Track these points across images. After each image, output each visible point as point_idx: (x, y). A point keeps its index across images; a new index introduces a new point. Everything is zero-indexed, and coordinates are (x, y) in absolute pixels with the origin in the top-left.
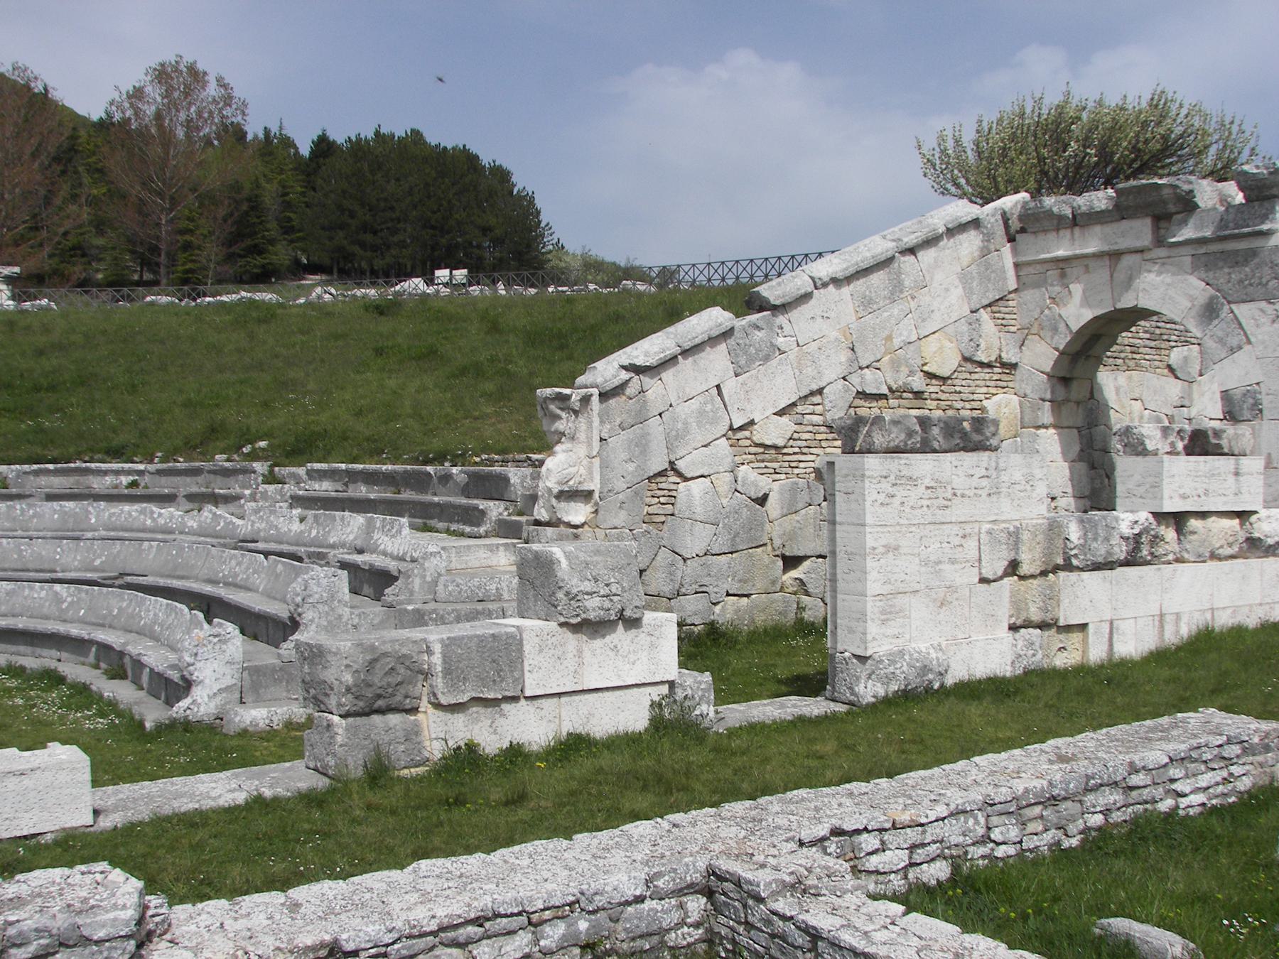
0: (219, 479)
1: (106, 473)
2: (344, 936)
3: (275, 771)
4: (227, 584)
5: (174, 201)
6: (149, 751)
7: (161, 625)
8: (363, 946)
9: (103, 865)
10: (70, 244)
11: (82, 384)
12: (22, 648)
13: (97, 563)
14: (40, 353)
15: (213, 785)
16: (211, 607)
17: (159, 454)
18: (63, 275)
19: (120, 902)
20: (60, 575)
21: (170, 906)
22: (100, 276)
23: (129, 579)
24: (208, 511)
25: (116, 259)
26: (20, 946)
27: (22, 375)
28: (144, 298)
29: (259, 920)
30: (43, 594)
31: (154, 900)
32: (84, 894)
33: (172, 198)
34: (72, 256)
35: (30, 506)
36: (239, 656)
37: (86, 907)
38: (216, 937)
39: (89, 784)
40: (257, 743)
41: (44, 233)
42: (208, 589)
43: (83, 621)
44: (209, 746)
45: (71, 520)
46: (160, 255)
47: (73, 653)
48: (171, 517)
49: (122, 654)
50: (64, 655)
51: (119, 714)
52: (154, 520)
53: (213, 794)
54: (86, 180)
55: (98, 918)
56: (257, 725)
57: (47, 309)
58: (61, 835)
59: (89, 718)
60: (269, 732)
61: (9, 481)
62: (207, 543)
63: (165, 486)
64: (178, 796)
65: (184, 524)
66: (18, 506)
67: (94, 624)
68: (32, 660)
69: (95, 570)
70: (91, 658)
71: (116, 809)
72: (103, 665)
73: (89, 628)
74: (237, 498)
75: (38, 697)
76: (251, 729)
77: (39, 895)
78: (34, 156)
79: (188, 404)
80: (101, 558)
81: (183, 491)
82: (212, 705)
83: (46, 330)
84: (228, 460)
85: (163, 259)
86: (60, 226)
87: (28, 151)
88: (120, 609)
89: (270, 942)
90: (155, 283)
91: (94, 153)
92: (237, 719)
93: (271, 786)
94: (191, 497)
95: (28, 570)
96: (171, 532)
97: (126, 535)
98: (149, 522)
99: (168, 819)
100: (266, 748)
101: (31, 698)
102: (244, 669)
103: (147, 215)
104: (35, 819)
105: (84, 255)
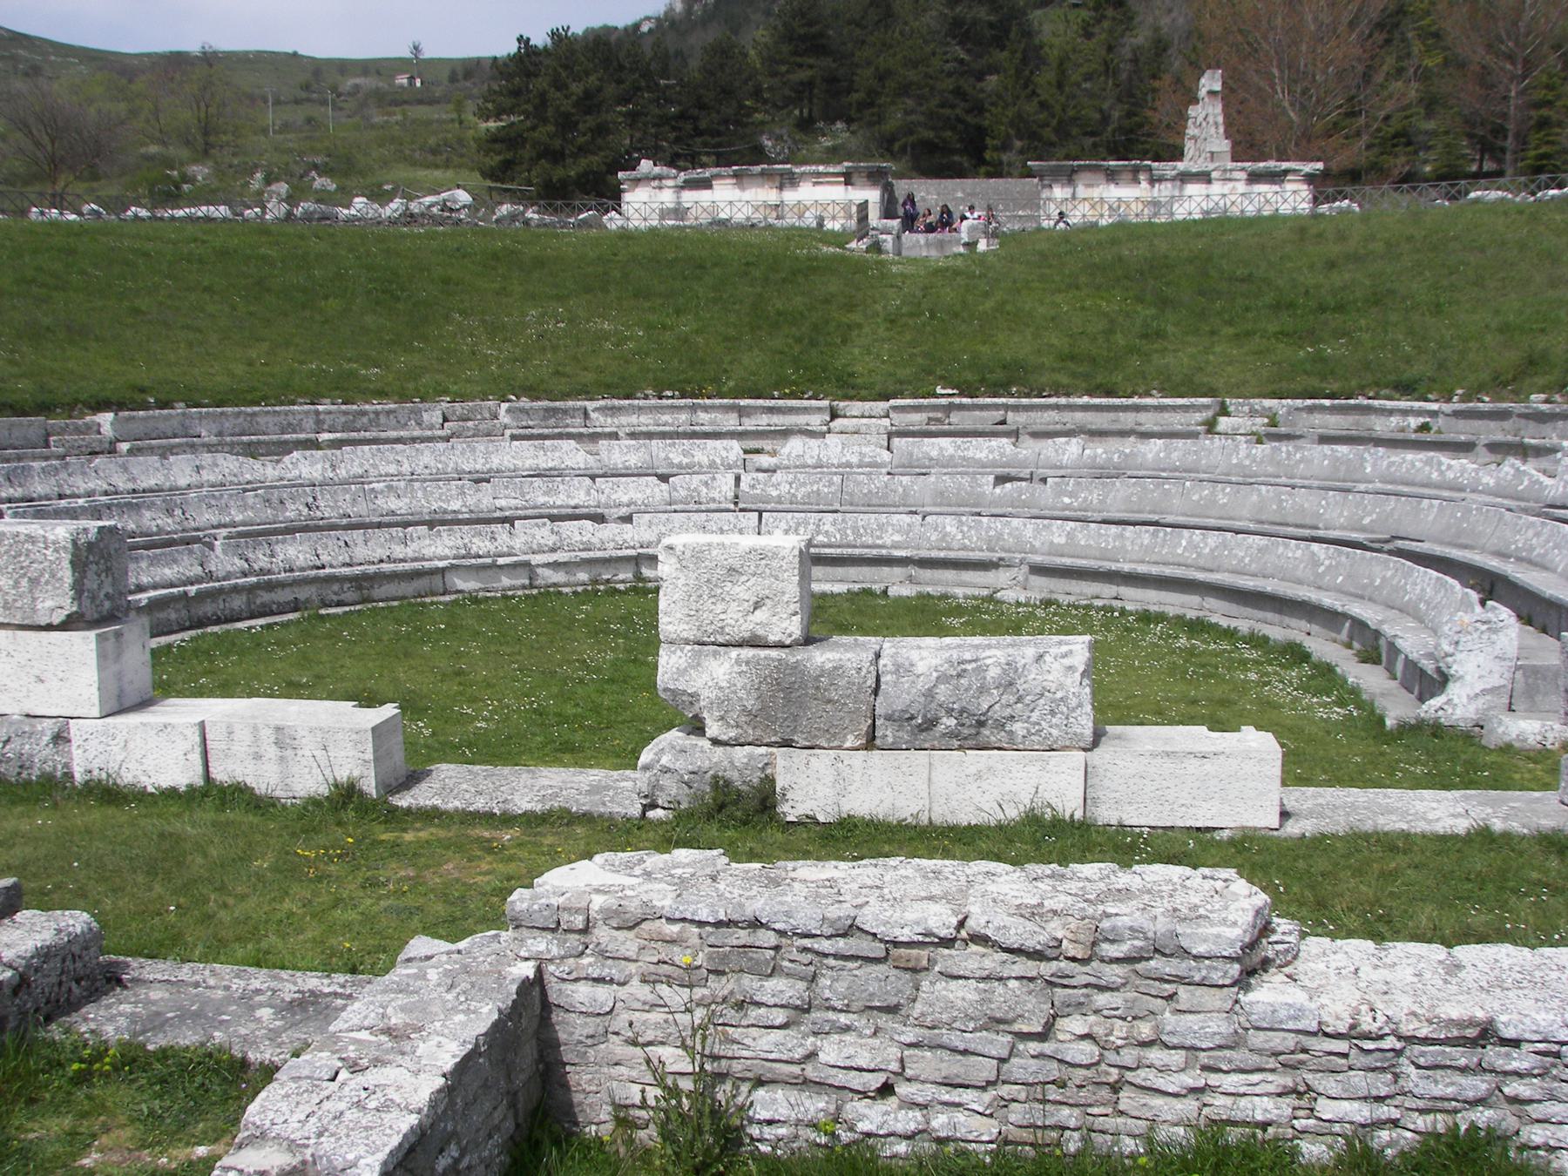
0: (1532, 424)
1: (1391, 412)
2: (1503, 1018)
3: (1516, 799)
4: (1519, 559)
5: (1528, 65)
6: (1382, 754)
7: (1428, 603)
8: (1527, 1036)
9: (1230, 873)
10: (1391, 130)
11: (1376, 303)
12: (1270, 616)
13: (1366, 521)
14: (1331, 265)
15: (1434, 805)
16: (1491, 586)
17: (1460, 391)
18: (1381, 170)
19: (1231, 918)
20: (1321, 533)
21: (1303, 935)
22: (1428, 169)
23: (1399, 543)
24: (1511, 465)
25: (1448, 145)
26: (1113, 942)
27: (1307, 292)
28: (1467, 193)
29: (1405, 974)
30: (1299, 553)
31: (1283, 925)
32: (1196, 900)
33: (1526, 61)
34: (1394, 146)
35: (1297, 449)
36: (1512, 651)
37: (1193, 915)
38: (1343, 983)
39: (1278, 781)
40: (1521, 763)
41: (1362, 120)
42: (1493, 564)
43: (1340, 590)
44: (1456, 756)
45: (1343, 468)
46: (1506, 137)
47: (1324, 626)
48: (1463, 470)
49: (1377, 634)
50: (1315, 628)
51: (1360, 705)
52: (1442, 473)
53: (1431, 816)
54: (1417, 47)
55: (1200, 930)
56: (1525, 740)
57: (1348, 211)
58: (1239, 834)
59: (1325, 705)
60: (1539, 752)
61: (1278, 418)
62: (1502, 506)
63: (1461, 431)
64: (1388, 811)
65: (1478, 481)
66: (1285, 447)
67: (1352, 595)
68: (1278, 630)
69: (1363, 529)
70: (1344, 635)
71: (1310, 814)
72: (1356, 645)
73: (1345, 599)
74: (1553, 450)
75: (1276, 673)
76: (1517, 745)
77: (1149, 892)
78: (1352, 25)
79: (1504, 329)
80: (1370, 515)
81: (1484, 439)
82: (1472, 708)
83: (1342, 237)
84: (1547, 401)
85: (1510, 143)
86: (1380, 108)
87: (1346, 18)
88: (1384, 579)
89: (1406, 1003)
90: (1500, 174)
91: (1428, 13)
92: (1500, 730)
93: (1505, 819)
94: (1493, 447)
95: (1287, 525)
96: (1461, 489)
97: (1406, 489)
98: (1435, 475)
99: (1366, 836)
100: (1530, 771)
101: (1267, 674)
102: (1518, 668)
103: (1493, 86)
104: (1214, 810)
105: (1409, 144)
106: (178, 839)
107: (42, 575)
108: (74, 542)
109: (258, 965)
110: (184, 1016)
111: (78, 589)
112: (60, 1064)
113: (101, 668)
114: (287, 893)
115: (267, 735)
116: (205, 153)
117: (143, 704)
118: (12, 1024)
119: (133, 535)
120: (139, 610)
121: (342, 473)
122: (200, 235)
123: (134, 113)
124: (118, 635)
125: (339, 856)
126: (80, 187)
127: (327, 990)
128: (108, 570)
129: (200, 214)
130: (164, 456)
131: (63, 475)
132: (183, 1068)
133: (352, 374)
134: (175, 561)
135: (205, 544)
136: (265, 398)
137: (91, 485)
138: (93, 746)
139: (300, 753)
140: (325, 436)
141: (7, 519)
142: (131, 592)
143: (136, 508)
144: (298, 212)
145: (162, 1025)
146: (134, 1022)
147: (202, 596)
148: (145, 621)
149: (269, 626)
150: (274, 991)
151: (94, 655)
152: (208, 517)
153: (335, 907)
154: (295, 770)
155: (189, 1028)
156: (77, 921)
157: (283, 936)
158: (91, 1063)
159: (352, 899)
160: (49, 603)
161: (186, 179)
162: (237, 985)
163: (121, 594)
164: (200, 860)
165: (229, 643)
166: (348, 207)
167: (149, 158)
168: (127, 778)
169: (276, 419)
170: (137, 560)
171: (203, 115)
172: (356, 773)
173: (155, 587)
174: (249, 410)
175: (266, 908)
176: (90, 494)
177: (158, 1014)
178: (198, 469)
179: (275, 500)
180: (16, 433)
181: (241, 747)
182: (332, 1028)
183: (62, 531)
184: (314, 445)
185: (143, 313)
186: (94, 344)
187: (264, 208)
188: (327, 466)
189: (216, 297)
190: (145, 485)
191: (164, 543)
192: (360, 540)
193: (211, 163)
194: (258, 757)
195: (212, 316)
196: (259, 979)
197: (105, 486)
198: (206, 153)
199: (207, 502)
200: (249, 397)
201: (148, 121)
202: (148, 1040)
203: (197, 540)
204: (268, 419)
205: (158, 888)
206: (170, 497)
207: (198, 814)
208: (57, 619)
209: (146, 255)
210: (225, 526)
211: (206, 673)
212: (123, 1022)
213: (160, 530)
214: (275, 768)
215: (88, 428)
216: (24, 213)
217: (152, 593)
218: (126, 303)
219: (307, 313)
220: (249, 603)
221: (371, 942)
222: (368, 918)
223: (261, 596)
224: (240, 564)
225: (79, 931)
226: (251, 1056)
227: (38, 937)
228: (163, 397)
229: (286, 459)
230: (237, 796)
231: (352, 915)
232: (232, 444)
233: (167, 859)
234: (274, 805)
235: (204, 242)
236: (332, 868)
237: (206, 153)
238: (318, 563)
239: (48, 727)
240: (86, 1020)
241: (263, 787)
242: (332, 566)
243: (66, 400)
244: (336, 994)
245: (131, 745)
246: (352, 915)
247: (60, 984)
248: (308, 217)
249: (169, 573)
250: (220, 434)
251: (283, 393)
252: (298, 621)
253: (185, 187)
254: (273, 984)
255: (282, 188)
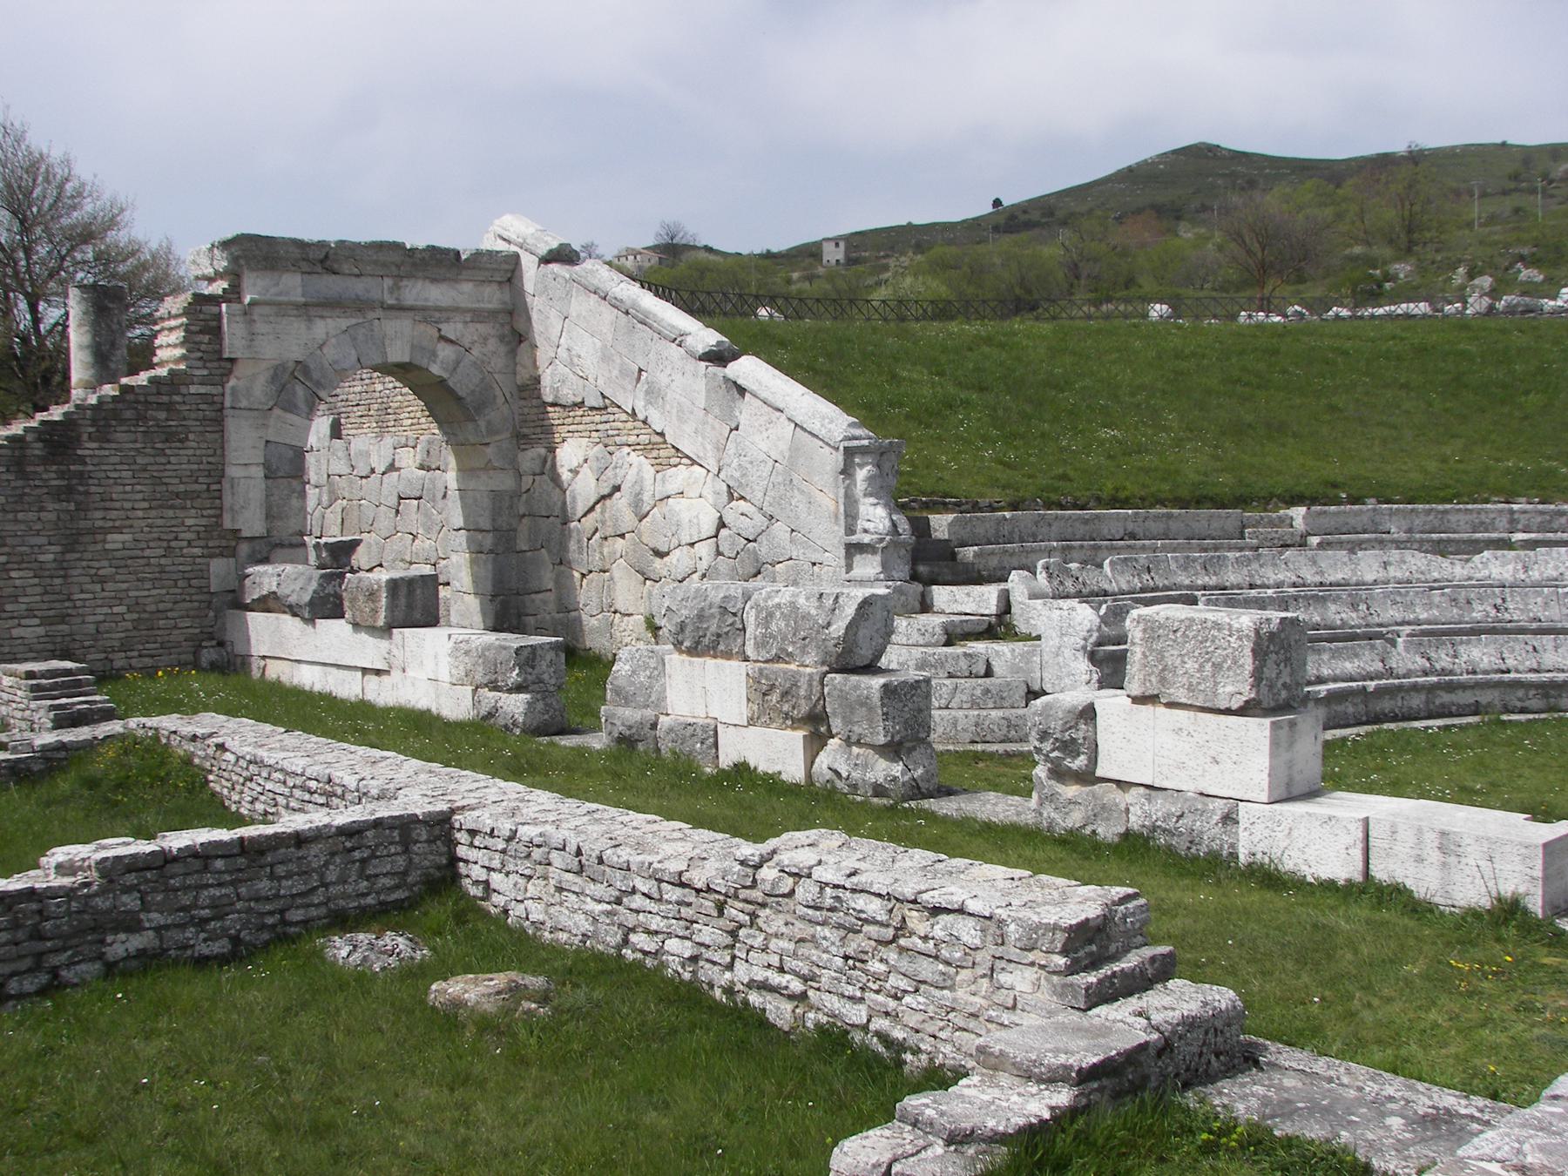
3: (251, 828)
106: (1331, 931)
107: (1225, 661)
108: (1257, 631)
109: (1395, 1072)
110: (1314, 1109)
111: (1257, 675)
112: (1191, 1131)
113: (1273, 755)
114: (1434, 1003)
115: (1431, 839)
116: (1408, 251)
117: (1311, 795)
118: (1153, 1084)
119: (1316, 627)
120: (1318, 701)
121: (1535, 575)
122: (1398, 332)
123: (1339, 216)
124: (1292, 724)
125: (1495, 974)
126: (1288, 290)
127: (1463, 1111)
128: (1287, 660)
129: (1399, 311)
130: (1352, 551)
131: (1255, 566)
132: (1306, 1160)
133: (1551, 473)
134: (1356, 655)
135: (1387, 640)
136: (1456, 496)
137: (1281, 577)
138: (1259, 830)
139: (1464, 860)
140: (1518, 536)
141: (1201, 606)
142: (1309, 683)
143: (1321, 600)
144: (1501, 305)
145: (1292, 1113)
146: (1265, 1105)
147: (1380, 692)
148: (1321, 713)
149: (1447, 728)
150: (1408, 1102)
151: (1267, 742)
152: (1393, 613)
153: (1483, 1026)
154: (1457, 877)
155: (1317, 1122)
156: (1223, 997)
157: (1425, 1047)
158: (1219, 1137)
159: (1503, 1021)
160: (1230, 689)
161: (1388, 277)
162: (1371, 1088)
163: (1298, 684)
164: (1349, 956)
165: (1404, 742)
166: (1554, 298)
167: (1354, 259)
168: (1288, 865)
169: (1468, 517)
170: (1319, 652)
171: (1407, 213)
172: (1522, 890)
173: (1335, 679)
174: (1440, 507)
175: (1411, 1015)
176: (1279, 585)
177: (1288, 1101)
178: (1386, 565)
179: (1462, 599)
180: (1215, 525)
181: (1404, 846)
182: (1460, 1152)
183: (1245, 620)
184: (1506, 545)
185: (1341, 411)
186: (1291, 440)
187: (1465, 303)
188: (1519, 567)
189: (1412, 394)
190: (1332, 579)
191: (1346, 637)
192: (1550, 646)
193: (1413, 260)
194: (1419, 860)
195: (1407, 412)
196: (1394, 1086)
197: (1294, 578)
198: (1409, 250)
199: (1392, 599)
200: (1442, 494)
201: (1353, 222)
202: (1276, 1126)
203: (1380, 636)
204: (1460, 517)
205: (1305, 978)
206: (1355, 592)
207: (1355, 910)
208: (1235, 704)
209: (1345, 353)
210: (1409, 623)
211: (1377, 770)
212: (1254, 1102)
213: (1344, 624)
214: (1438, 874)
215: (1281, 520)
216: (1234, 317)
217: (1332, 686)
218: (1324, 401)
219: (1506, 410)
220: (1427, 702)
221: (1518, 1069)
222: (1519, 1045)
223: (1440, 696)
224: (1421, 662)
225: (1223, 1007)
226: (1375, 1163)
227: (1185, 1006)
228: (1353, 492)
229: (1476, 558)
230: (1394, 896)
231: (1502, 1038)
232: (1421, 541)
233: (1317, 950)
234: (1431, 911)
235: (1402, 339)
236: (1485, 984)
237: (1409, 250)
238: (1503, 667)
239: (1219, 807)
240: (1220, 1093)
241: (1422, 891)
242: (1517, 671)
243: (1262, 494)
244: (1472, 1117)
245: (1295, 833)
246: (1502, 1038)
247: (1201, 1055)
248: (1511, 310)
249: (1349, 667)
250: (1410, 531)
251: (1477, 491)
252: (1476, 726)
253: (1388, 285)
254: (1407, 1094)
255: (1486, 281)
